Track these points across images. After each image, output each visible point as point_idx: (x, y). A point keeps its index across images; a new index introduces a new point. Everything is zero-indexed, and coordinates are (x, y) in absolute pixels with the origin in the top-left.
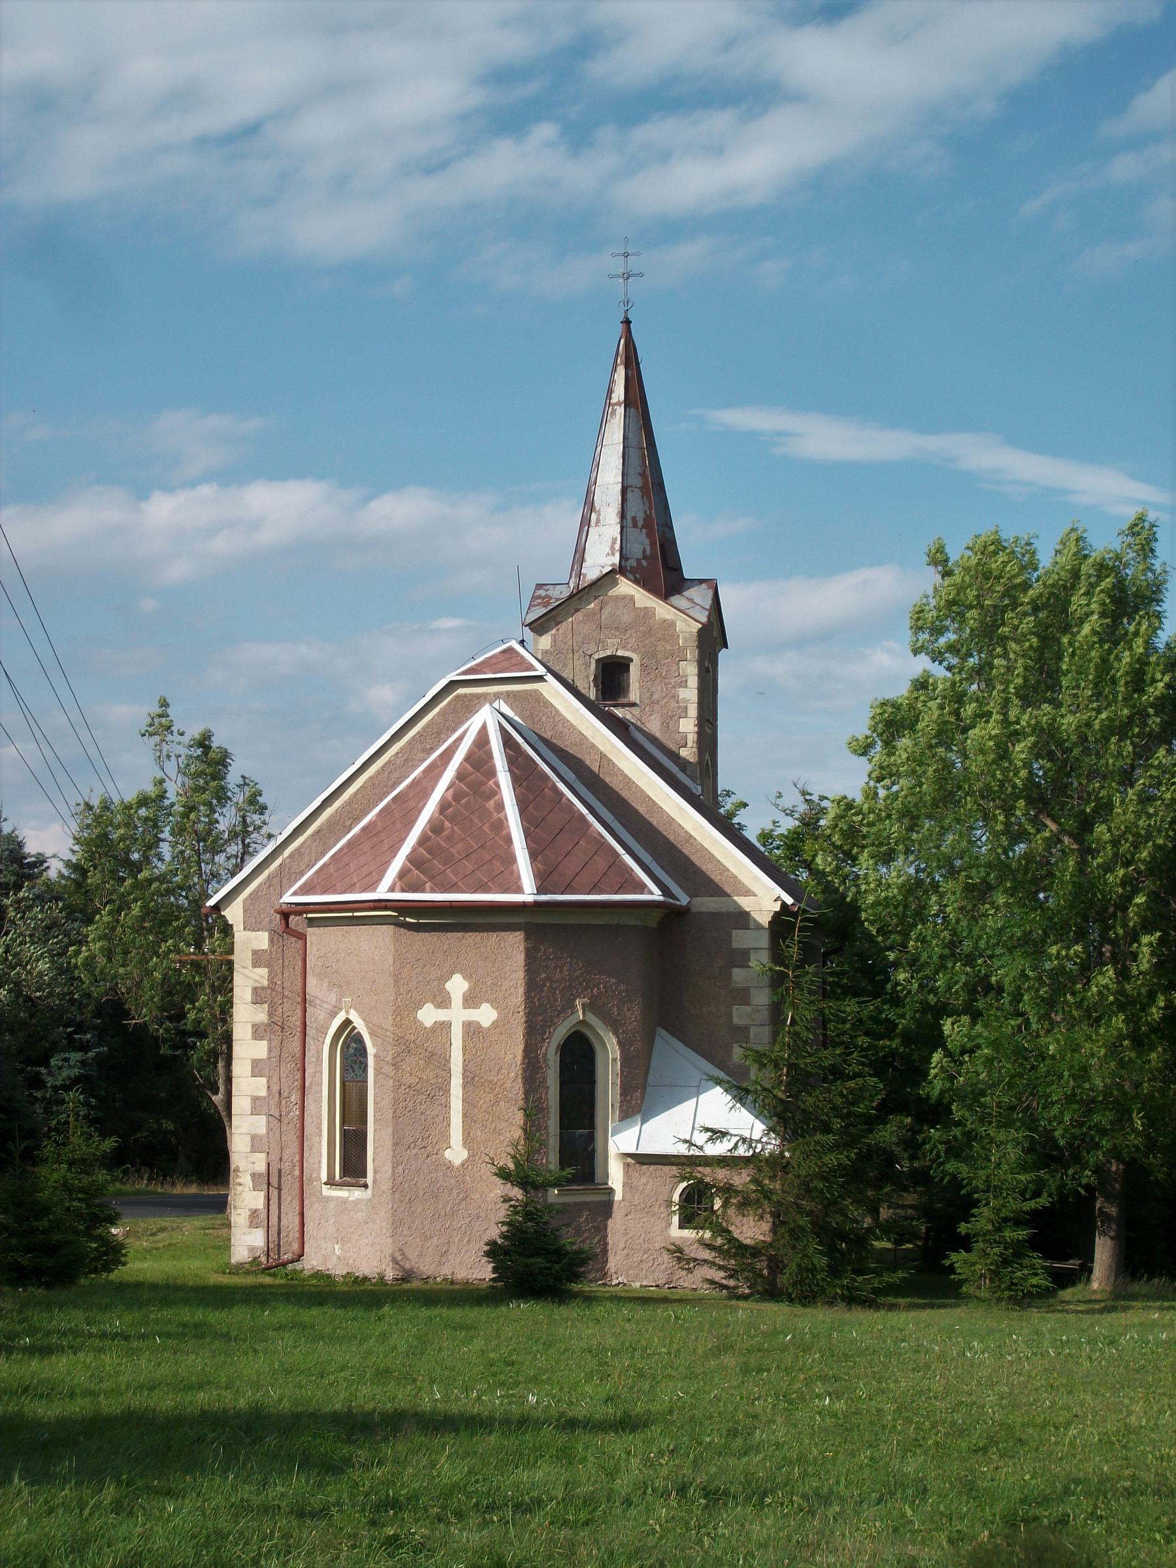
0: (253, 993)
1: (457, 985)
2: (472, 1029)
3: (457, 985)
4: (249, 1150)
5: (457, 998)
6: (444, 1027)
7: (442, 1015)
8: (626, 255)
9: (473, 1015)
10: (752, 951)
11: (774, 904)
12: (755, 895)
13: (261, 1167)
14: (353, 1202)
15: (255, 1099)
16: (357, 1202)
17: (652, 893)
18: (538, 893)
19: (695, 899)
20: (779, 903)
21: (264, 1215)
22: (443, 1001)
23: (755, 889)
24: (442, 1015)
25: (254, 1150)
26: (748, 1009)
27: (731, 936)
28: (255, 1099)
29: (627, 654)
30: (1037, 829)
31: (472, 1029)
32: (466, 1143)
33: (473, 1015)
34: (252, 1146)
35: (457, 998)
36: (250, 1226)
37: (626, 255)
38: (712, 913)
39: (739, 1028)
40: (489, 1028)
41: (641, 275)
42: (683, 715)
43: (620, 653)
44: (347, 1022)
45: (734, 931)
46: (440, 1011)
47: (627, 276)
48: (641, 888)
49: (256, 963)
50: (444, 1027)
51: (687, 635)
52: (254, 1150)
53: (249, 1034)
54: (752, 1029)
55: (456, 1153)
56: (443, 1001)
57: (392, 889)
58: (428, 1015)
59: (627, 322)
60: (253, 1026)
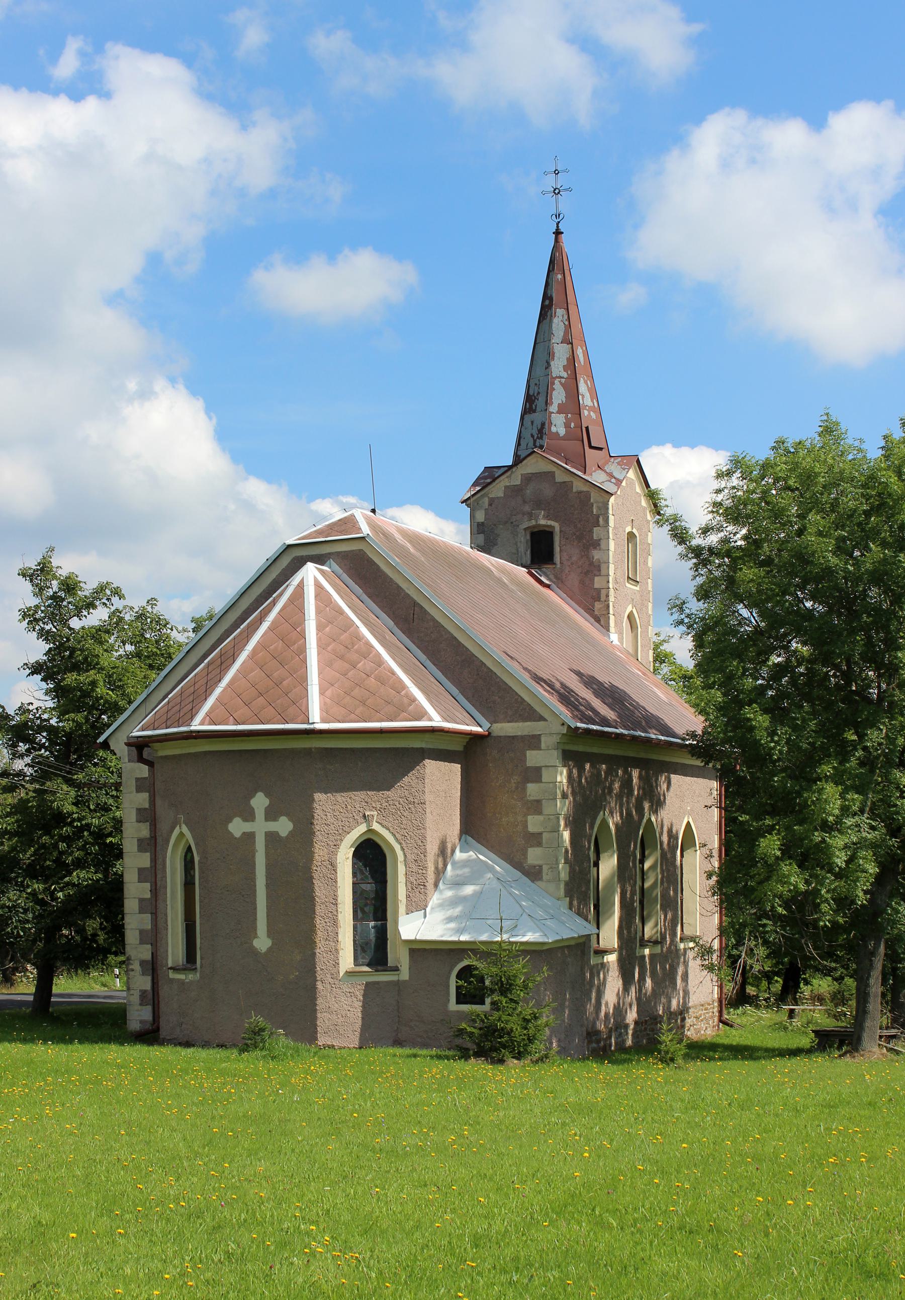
0: (137, 814)
1: (260, 802)
2: (272, 838)
3: (260, 802)
4: (138, 942)
5: (260, 814)
6: (249, 837)
7: (247, 827)
8: (556, 172)
9: (272, 826)
10: (543, 768)
11: (561, 728)
12: (545, 720)
13: (148, 956)
14: (188, 983)
15: (141, 901)
16: (191, 982)
17: (431, 719)
18: (794, 1009)
19: (495, 725)
20: (565, 728)
21: (150, 996)
22: (249, 816)
23: (546, 716)
24: (247, 827)
25: (142, 942)
26: (541, 818)
27: (525, 756)
28: (141, 901)
29: (550, 523)
30: (799, 659)
31: (272, 838)
32: (270, 934)
33: (272, 826)
34: (140, 939)
35: (260, 814)
36: (141, 1005)
37: (556, 172)
38: (509, 737)
39: (533, 834)
40: (287, 837)
41: (569, 190)
42: (598, 573)
43: (543, 522)
44: (182, 834)
45: (528, 753)
46: (247, 823)
47: (556, 192)
48: (421, 714)
49: (139, 789)
50: (249, 837)
51: (600, 505)
52: (142, 942)
53: (135, 848)
54: (545, 836)
55: (262, 942)
56: (249, 816)
57: (202, 723)
58: (237, 827)
59: (558, 233)
60: (138, 840)
